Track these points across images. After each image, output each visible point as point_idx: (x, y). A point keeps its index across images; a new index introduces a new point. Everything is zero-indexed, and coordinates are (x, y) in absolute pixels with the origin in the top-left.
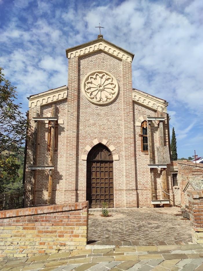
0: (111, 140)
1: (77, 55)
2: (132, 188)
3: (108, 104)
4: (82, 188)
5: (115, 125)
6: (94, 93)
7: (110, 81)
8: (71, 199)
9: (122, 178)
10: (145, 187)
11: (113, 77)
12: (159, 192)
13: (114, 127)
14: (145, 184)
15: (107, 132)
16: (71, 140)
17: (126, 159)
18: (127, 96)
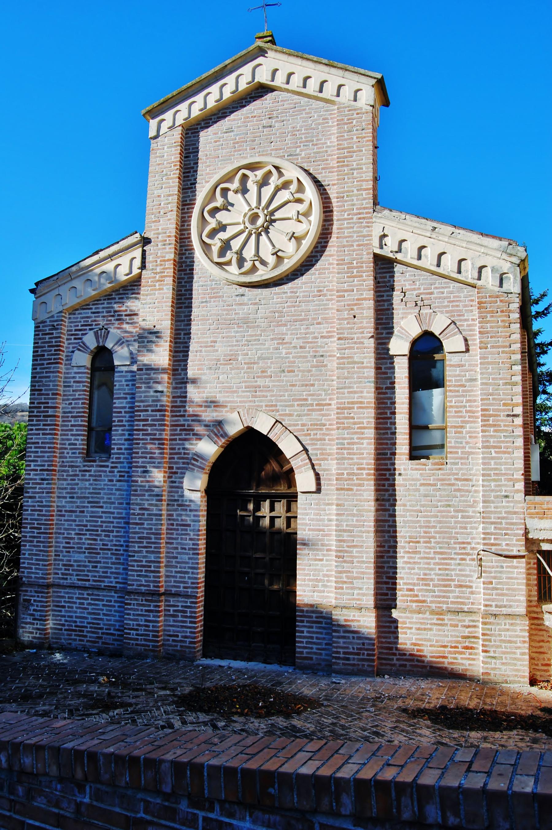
0: (291, 415)
1: (180, 119)
2: (358, 600)
3: (282, 279)
4: (185, 587)
5: (306, 357)
6: (249, 253)
7: (274, 181)
8: (146, 621)
9: (324, 562)
10: (417, 601)
11: (278, 162)
12: (473, 621)
13: (304, 366)
14: (415, 588)
15: (274, 386)
16: (147, 420)
17: (342, 489)
18: (353, 241)
